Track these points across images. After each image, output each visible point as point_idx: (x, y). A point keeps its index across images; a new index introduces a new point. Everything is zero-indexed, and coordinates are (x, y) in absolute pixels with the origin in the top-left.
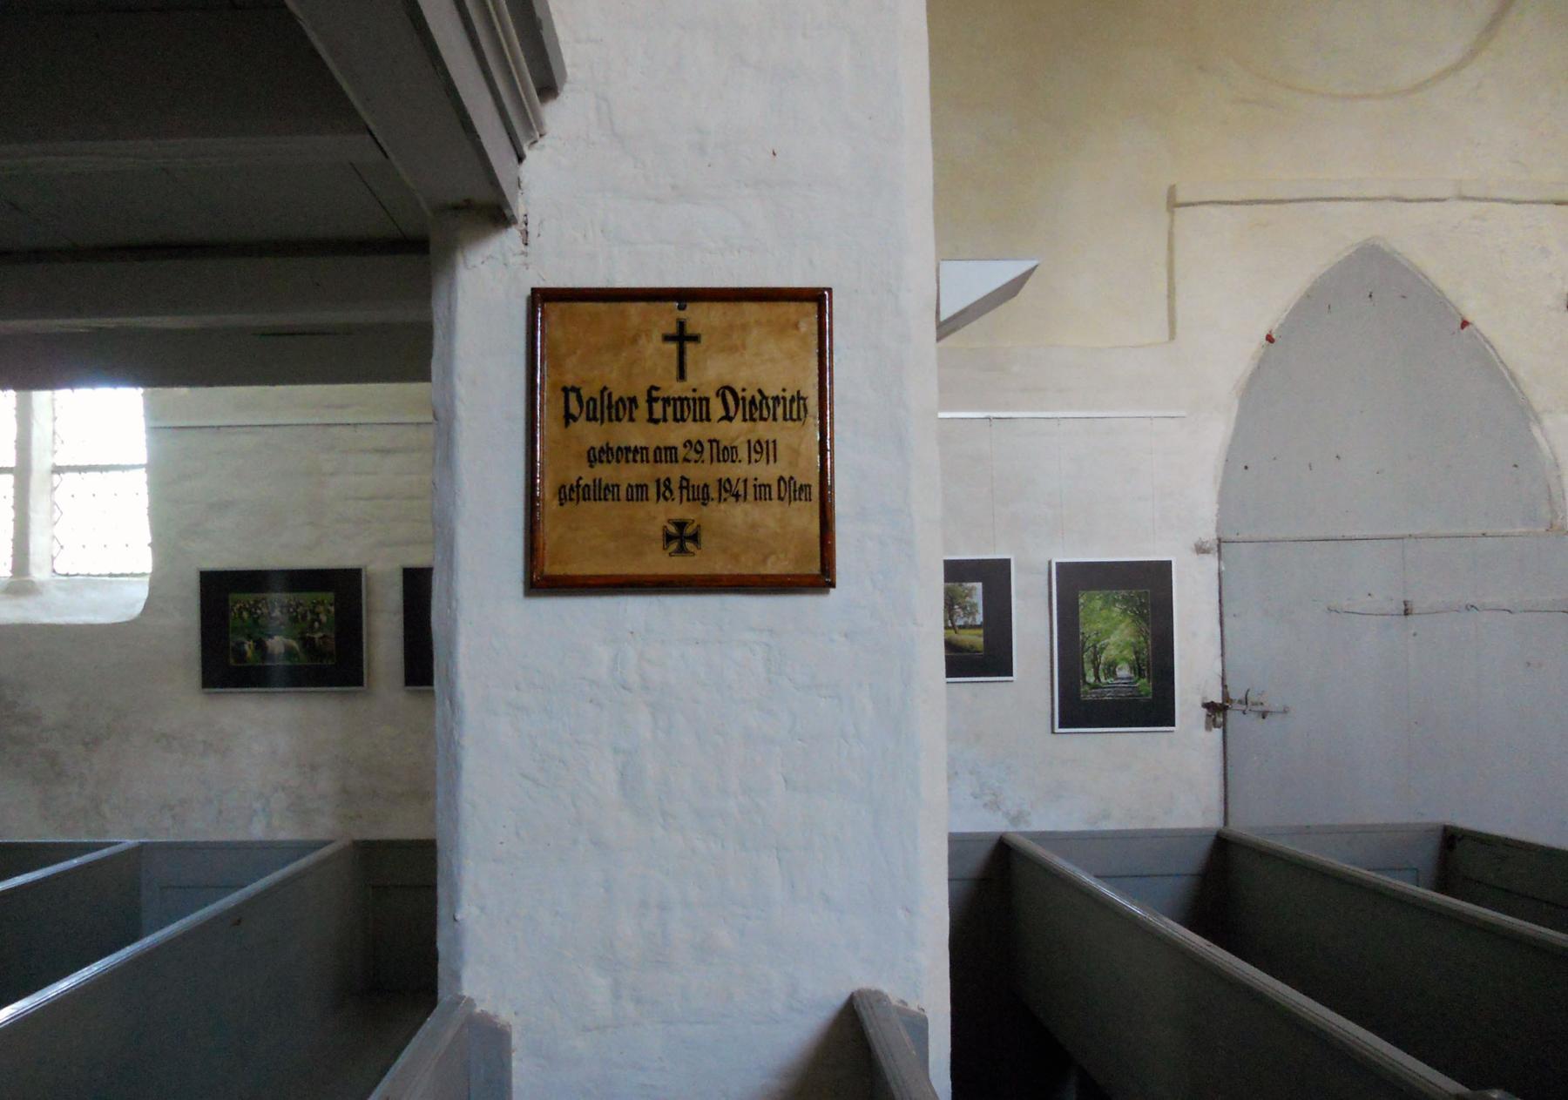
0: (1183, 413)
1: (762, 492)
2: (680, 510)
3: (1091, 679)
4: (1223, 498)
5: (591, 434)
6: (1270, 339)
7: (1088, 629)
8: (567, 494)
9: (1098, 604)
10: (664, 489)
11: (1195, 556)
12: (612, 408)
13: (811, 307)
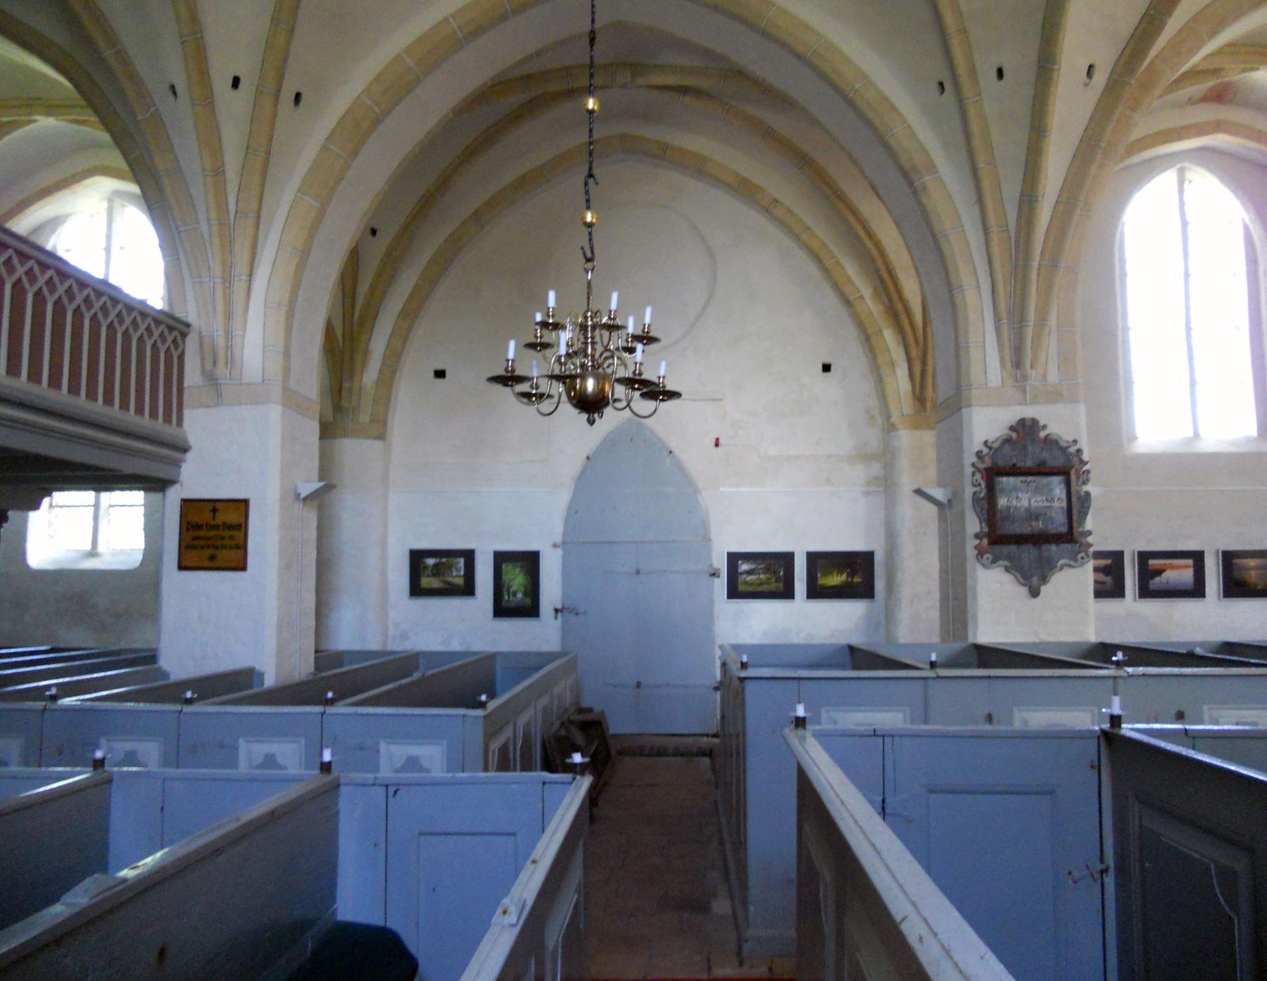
1: (231, 548)
2: (211, 551)
3: (506, 598)
5: (193, 533)
6: (588, 458)
7: (506, 578)
8: (188, 547)
10: (209, 547)
12: (198, 527)
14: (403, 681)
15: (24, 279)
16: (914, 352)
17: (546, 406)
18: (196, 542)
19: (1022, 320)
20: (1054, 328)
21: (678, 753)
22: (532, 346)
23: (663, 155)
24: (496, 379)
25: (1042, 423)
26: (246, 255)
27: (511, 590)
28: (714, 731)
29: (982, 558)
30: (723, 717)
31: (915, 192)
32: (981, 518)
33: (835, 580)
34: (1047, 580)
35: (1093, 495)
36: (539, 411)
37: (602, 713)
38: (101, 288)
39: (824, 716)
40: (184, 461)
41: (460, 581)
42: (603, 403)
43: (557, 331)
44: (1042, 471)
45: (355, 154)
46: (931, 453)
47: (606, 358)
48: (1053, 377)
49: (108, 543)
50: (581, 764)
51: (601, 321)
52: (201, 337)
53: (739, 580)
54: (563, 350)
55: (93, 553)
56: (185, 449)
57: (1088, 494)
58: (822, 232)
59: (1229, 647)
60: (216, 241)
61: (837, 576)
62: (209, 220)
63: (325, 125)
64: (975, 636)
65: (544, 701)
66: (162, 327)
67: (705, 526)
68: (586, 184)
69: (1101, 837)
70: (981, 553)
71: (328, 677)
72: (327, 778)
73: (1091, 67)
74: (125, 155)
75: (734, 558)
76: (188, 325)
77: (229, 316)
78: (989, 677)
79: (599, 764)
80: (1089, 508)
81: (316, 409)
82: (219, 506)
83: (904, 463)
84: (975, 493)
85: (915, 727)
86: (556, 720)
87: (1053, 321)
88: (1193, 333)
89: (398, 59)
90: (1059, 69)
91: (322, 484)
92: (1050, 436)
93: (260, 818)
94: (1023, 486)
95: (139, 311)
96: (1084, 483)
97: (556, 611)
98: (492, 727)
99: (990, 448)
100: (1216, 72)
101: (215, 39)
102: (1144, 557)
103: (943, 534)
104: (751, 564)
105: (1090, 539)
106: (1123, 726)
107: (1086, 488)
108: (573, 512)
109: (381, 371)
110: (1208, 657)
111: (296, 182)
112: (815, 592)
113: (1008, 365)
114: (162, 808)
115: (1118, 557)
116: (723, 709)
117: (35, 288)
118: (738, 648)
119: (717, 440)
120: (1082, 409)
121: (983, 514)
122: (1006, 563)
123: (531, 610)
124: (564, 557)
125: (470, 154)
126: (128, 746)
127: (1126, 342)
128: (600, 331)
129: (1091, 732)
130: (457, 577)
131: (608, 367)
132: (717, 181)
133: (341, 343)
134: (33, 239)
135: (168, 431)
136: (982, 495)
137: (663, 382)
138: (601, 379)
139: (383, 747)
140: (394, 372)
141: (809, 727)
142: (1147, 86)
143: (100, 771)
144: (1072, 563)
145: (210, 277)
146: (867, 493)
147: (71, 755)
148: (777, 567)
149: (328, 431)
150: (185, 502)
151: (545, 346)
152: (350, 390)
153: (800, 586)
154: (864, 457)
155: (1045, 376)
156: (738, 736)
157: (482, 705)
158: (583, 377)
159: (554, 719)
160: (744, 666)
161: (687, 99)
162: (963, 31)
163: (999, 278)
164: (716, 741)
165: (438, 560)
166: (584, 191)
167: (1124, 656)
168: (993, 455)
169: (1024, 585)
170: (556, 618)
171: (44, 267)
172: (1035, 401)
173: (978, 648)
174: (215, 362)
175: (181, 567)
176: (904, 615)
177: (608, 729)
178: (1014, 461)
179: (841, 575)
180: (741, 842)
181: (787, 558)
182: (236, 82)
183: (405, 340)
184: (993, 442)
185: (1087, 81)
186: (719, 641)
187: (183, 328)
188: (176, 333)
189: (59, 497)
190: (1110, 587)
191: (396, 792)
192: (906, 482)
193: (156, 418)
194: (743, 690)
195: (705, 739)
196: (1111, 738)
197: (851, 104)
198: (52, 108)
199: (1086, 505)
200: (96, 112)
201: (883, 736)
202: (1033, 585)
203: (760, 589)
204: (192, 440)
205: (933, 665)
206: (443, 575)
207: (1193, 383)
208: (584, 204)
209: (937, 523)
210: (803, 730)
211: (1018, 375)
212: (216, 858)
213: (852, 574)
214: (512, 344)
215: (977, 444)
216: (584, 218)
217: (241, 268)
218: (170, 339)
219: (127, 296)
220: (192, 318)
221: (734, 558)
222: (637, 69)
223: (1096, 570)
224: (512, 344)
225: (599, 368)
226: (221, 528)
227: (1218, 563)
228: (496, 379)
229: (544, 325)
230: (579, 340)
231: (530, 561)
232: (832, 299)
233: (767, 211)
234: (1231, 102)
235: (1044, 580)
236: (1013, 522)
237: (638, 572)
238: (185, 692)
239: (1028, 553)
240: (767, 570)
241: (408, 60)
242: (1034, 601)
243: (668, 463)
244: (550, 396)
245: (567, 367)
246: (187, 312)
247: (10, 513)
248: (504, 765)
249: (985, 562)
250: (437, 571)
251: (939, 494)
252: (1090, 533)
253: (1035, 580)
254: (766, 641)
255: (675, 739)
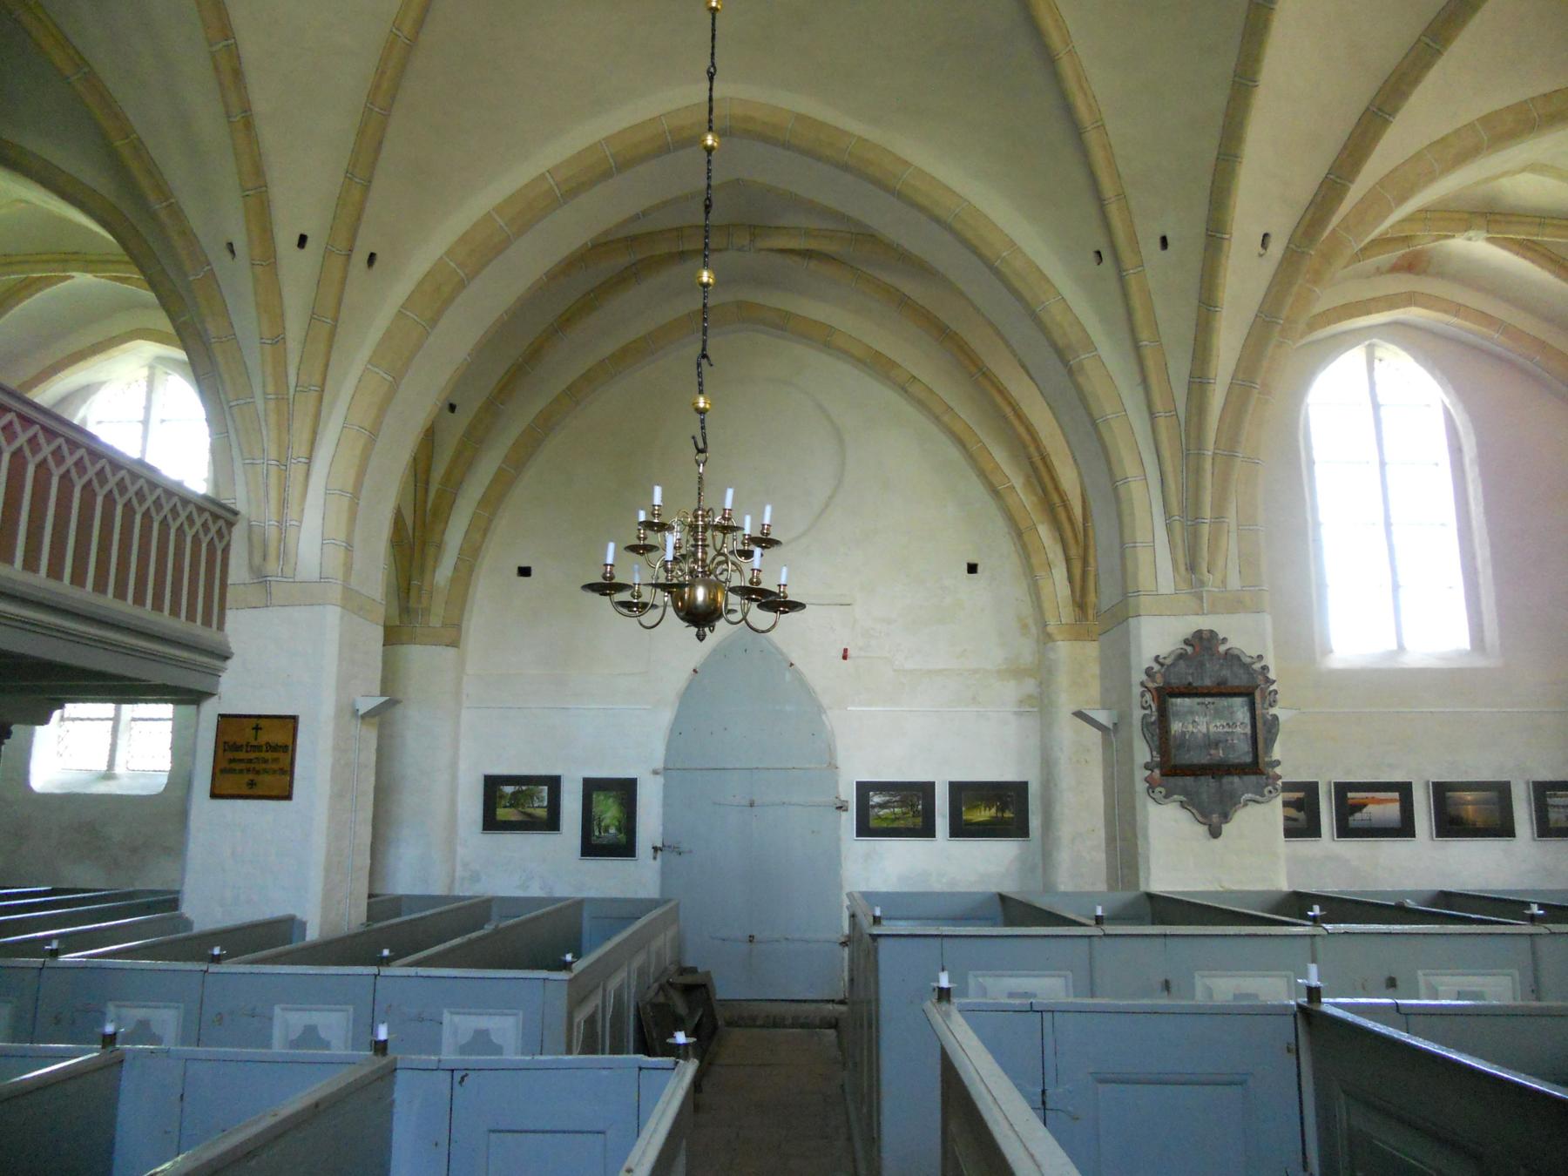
0: (649, 707)
1: (274, 772)
2: (251, 776)
3: (597, 833)
4: (668, 749)
5: (230, 755)
6: (695, 671)
7: (596, 810)
8: (223, 771)
9: (602, 798)
10: (248, 770)
11: (652, 776)
12: (236, 748)
13: (292, 721)
14: (474, 935)
15: (50, 459)
16: (1074, 552)
17: (650, 617)
18: (233, 765)
19: (1197, 520)
20: (1233, 527)
21: (798, 1023)
22: (633, 549)
23: (784, 325)
24: (592, 587)
25: (1221, 636)
26: (306, 435)
27: (603, 824)
28: (842, 997)
29: (1153, 792)
30: (852, 980)
31: (1070, 372)
32: (1152, 745)
33: (983, 815)
34: (1229, 818)
35: (1281, 719)
36: (641, 624)
37: (708, 974)
38: (137, 469)
39: (972, 982)
40: (223, 670)
41: (542, 813)
42: (715, 616)
43: (662, 533)
44: (1222, 691)
45: (434, 322)
46: (1094, 669)
47: (720, 563)
48: (1234, 582)
49: (127, 762)
50: (686, 1045)
51: (714, 521)
52: (250, 526)
53: (871, 813)
54: (669, 556)
55: (109, 775)
56: (225, 657)
57: (1275, 718)
58: (966, 414)
59: (1445, 898)
60: (273, 419)
61: (985, 810)
62: (265, 393)
63: (401, 290)
64: (1148, 884)
65: (638, 962)
66: (207, 515)
67: (831, 750)
68: (699, 365)
69: (1302, 1118)
70: (1151, 786)
71: (381, 929)
72: (382, 1061)
73: (1266, 236)
74: (173, 319)
75: (864, 789)
76: (236, 513)
77: (283, 503)
78: (1165, 935)
79: (707, 1036)
80: (1277, 735)
81: (380, 612)
82: (262, 723)
83: (1062, 679)
84: (1144, 717)
85: (1079, 1000)
86: (654, 982)
87: (1231, 517)
88: (1393, 528)
89: (488, 217)
90: (1229, 240)
91: (383, 699)
92: (1230, 651)
93: (304, 1111)
94: (1197, 708)
95: (175, 497)
96: (1271, 706)
97: (656, 849)
98: (579, 993)
99: (1162, 665)
100: (1406, 239)
101: (280, 195)
102: (1342, 789)
103: (1108, 764)
104: (884, 796)
105: (1278, 770)
106: (1323, 1000)
107: (1273, 711)
108: (676, 732)
109: (456, 568)
110: (1418, 910)
111: (365, 354)
112: (960, 829)
113: (1182, 568)
114: (182, 1095)
115: (1311, 789)
116: (851, 970)
117: (63, 469)
118: (869, 896)
119: (846, 650)
120: (1267, 619)
121: (1153, 741)
122: (1182, 798)
123: (624, 848)
124: (666, 787)
125: (565, 322)
126: (140, 1013)
127: (1317, 540)
128: (713, 532)
129: (1288, 1006)
130: (540, 809)
131: (721, 574)
132: (844, 354)
133: (411, 532)
134: (58, 411)
135: (208, 635)
136: (1153, 719)
137: (783, 592)
138: (712, 587)
139: (447, 1017)
140: (471, 570)
141: (954, 1000)
142: (1327, 258)
143: (110, 1048)
144: (1258, 798)
145: (264, 459)
146: (1018, 714)
147: (78, 1025)
148: (915, 799)
149: (392, 636)
150: (224, 718)
151: (649, 548)
152: (420, 588)
153: (942, 822)
154: (1017, 673)
155: (1224, 582)
156: (869, 1002)
157: (566, 966)
158: (692, 586)
159: (652, 981)
160: (877, 920)
161: (813, 264)
162: (1122, 196)
163: (1168, 467)
164: (843, 1008)
165: (517, 787)
166: (696, 372)
167: (1321, 910)
168: (1165, 672)
169: (1204, 824)
170: (655, 858)
171: (74, 445)
172: (1213, 612)
173: (1151, 897)
174: (265, 558)
175: (214, 795)
176: (1064, 857)
177: (715, 995)
178: (1190, 679)
179: (990, 810)
180: (873, 1138)
181: (927, 789)
182: (303, 240)
183: (486, 531)
184: (1165, 658)
185: (1262, 252)
186: (847, 889)
187: (229, 516)
188: (221, 523)
189: (71, 709)
190: (1302, 825)
191: (462, 1079)
192: (1066, 703)
193: (194, 621)
194: (876, 950)
195: (830, 1006)
196: (1309, 1016)
197: (996, 272)
198: (88, 265)
199: (1273, 731)
200: (142, 270)
201: (1041, 1012)
202: (1214, 818)
203: (895, 825)
204: (234, 646)
205: (1099, 920)
206: (523, 806)
207: (1396, 587)
208: (696, 388)
209: (1101, 749)
210: (947, 1005)
211: (1194, 580)
212: (248, 1161)
213: (1002, 809)
214: (611, 546)
215: (1146, 660)
216: (695, 403)
217: (299, 450)
218: (213, 529)
219: (165, 478)
220: (240, 506)
221: (864, 789)
222: (755, 230)
223: (1286, 804)
224: (611, 546)
225: (710, 575)
226: (264, 748)
227: (1431, 818)
228: (592, 587)
229: (648, 525)
230: (688, 541)
231: (626, 790)
232: (977, 489)
233: (903, 389)
234: (1424, 272)
235: (1226, 817)
236: (1189, 750)
237: (752, 805)
238: (212, 948)
239: (1207, 785)
240: (903, 803)
241: (498, 219)
242: (1215, 841)
243: (788, 676)
244: (654, 606)
245: (674, 574)
246: (235, 499)
247: (14, 728)
248: (590, 1047)
249: (1157, 796)
250: (515, 801)
251: (1102, 717)
252: (1278, 763)
253: (1215, 818)
254: (905, 889)
255: (794, 1006)
